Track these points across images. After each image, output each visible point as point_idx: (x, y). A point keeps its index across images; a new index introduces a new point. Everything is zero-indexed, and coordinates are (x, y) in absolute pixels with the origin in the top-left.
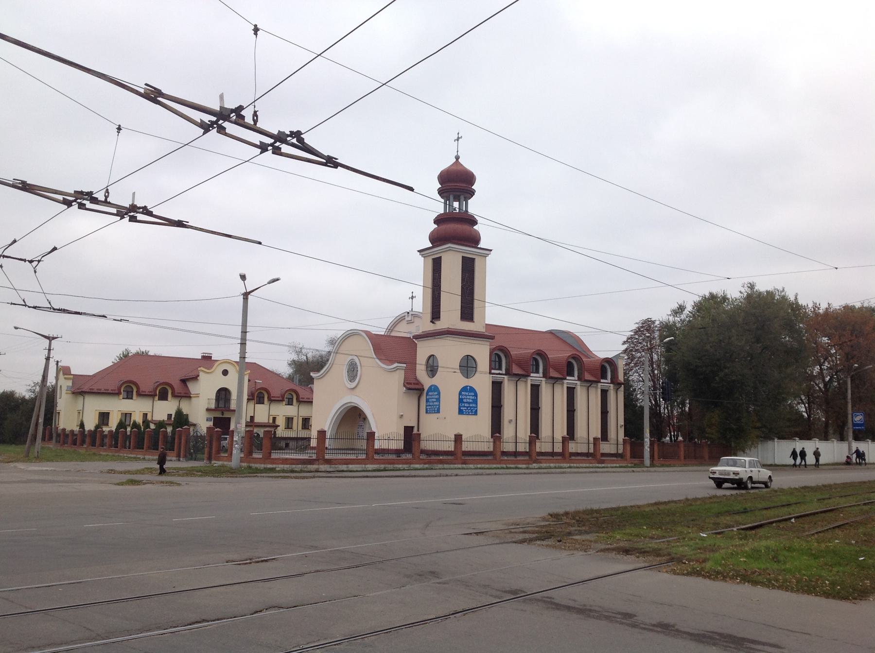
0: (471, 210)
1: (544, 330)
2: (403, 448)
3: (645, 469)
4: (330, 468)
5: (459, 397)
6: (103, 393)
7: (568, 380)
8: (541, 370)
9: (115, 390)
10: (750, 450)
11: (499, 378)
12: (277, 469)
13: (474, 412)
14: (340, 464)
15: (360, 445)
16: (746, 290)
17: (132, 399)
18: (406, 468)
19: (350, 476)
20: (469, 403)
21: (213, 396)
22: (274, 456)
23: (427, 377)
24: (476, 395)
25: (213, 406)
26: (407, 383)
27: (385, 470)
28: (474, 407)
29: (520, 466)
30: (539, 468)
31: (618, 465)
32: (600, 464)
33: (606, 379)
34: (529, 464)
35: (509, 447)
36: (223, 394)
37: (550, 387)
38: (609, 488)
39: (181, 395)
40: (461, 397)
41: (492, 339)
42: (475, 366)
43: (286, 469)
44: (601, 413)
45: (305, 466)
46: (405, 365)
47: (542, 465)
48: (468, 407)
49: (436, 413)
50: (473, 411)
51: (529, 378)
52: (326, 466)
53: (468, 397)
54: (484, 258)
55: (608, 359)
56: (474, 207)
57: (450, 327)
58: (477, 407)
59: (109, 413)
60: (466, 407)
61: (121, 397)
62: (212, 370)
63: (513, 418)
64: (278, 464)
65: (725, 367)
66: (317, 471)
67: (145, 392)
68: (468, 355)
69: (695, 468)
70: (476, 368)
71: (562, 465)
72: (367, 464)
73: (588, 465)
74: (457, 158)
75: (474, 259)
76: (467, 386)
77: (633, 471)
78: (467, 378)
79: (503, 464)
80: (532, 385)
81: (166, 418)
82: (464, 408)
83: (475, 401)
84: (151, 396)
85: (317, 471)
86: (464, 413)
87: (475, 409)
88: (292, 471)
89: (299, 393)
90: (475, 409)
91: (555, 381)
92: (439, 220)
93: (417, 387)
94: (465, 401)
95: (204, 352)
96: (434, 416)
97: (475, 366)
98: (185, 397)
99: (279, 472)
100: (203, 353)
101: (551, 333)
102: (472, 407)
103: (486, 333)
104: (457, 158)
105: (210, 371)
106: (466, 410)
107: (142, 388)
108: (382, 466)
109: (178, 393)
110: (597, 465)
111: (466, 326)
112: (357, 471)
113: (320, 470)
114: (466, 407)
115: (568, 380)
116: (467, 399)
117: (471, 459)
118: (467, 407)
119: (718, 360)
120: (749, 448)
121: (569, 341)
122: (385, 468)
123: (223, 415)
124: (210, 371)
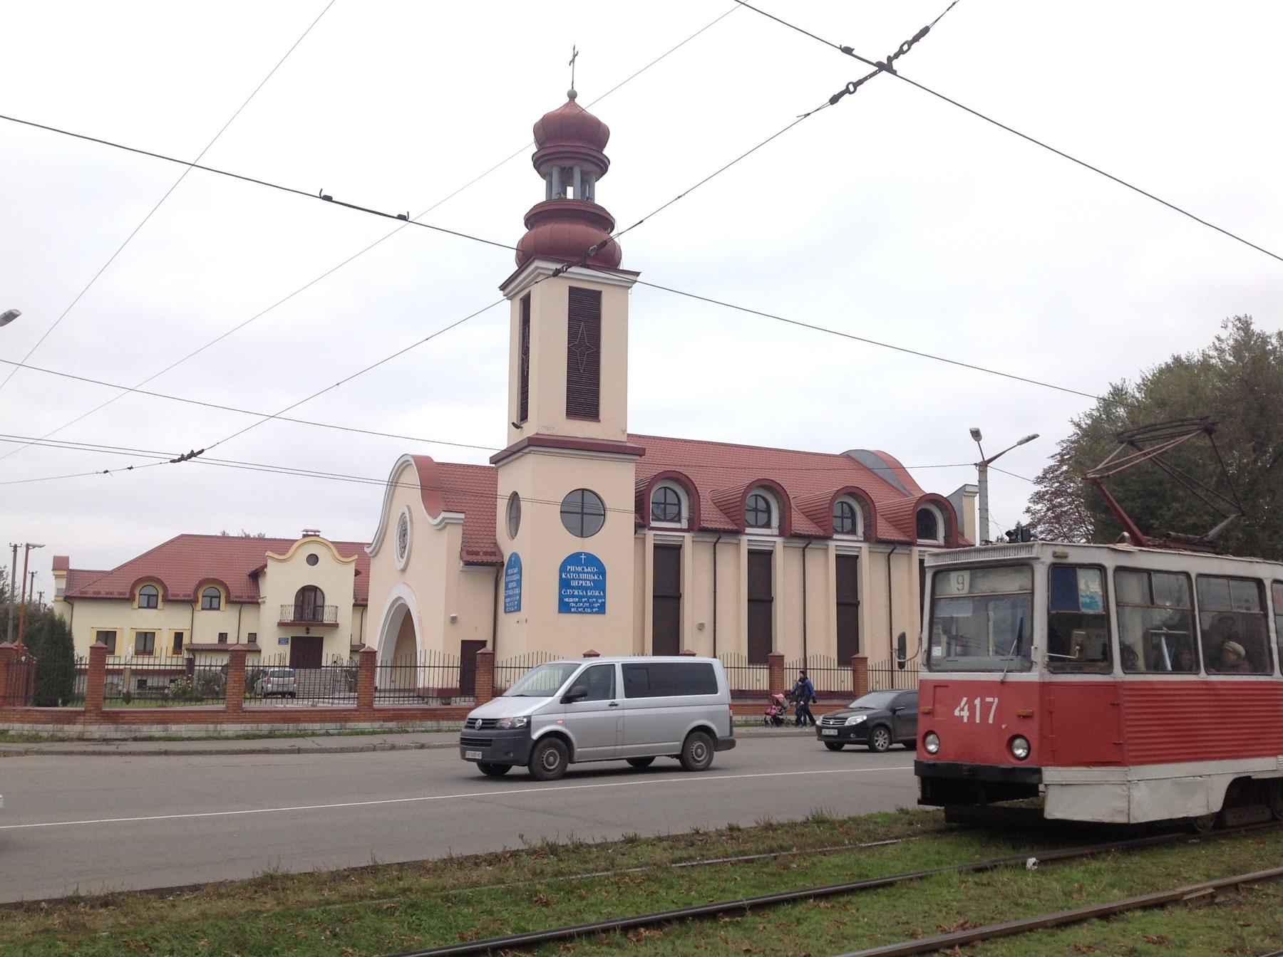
1: (838, 453)
2: (458, 686)
4: (116, 731)
5: (561, 576)
6: (115, 599)
7: (836, 540)
8: (775, 521)
11: (671, 538)
12: (11, 733)
13: (598, 607)
14: (146, 723)
15: (504, 680)
16: (1230, 336)
18: (331, 732)
20: (586, 589)
21: (291, 601)
22: (248, 705)
24: (602, 571)
25: (290, 617)
26: (469, 553)
27: (271, 735)
28: (597, 597)
33: (935, 538)
36: (309, 599)
38: (808, 772)
39: (241, 600)
40: (564, 576)
41: (641, 456)
42: (603, 513)
43: (25, 733)
45: (60, 726)
46: (462, 516)
50: (596, 605)
54: (623, 290)
55: (936, 498)
58: (604, 597)
60: (576, 596)
61: (136, 605)
62: (287, 556)
63: (707, 620)
64: (12, 721)
65: (1175, 499)
67: (177, 595)
68: (583, 490)
70: (604, 515)
72: (221, 723)
74: (572, 95)
75: (600, 293)
76: (580, 554)
78: (582, 536)
80: (750, 552)
81: (216, 641)
82: (571, 600)
83: (601, 585)
84: (190, 602)
86: (573, 610)
87: (600, 601)
88: (36, 739)
89: (149, 575)
90: (600, 601)
91: (805, 541)
92: (534, 218)
93: (493, 559)
94: (574, 583)
96: (514, 617)
97: (603, 513)
98: (249, 603)
99: (13, 740)
101: (847, 456)
102: (592, 597)
103: (628, 444)
104: (572, 95)
105: (282, 557)
106: (576, 603)
107: (234, 593)
108: (265, 727)
109: (236, 597)
112: (189, 739)
113: (87, 735)
114: (576, 596)
115: (836, 540)
118: (581, 597)
119: (1160, 483)
121: (886, 475)
122: (270, 732)
123: (308, 633)
124: (282, 557)
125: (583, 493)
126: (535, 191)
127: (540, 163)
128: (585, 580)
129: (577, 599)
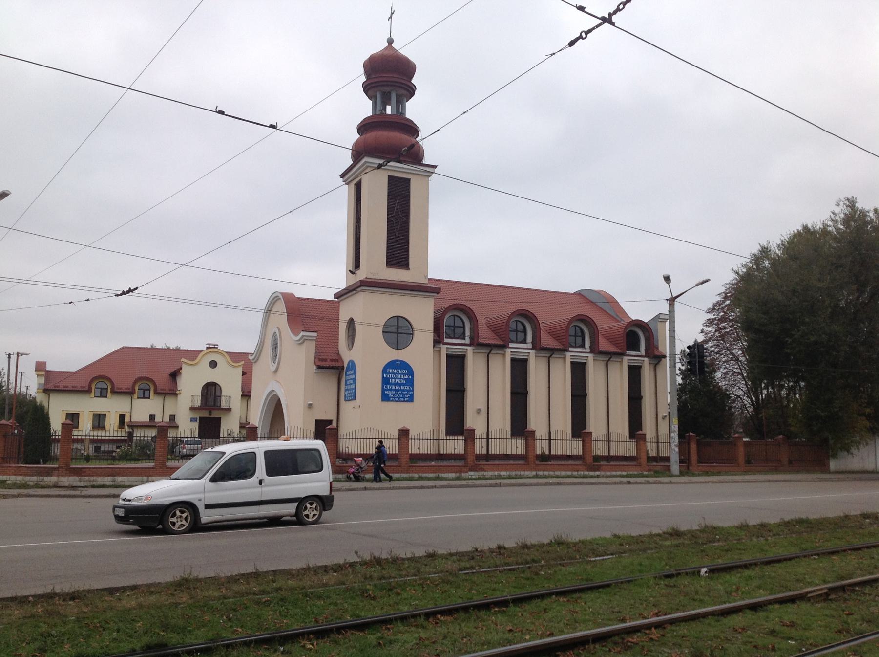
0: (409, 114)
3: (674, 479)
4: (80, 481)
6: (78, 391)
8: (529, 338)
9: (84, 387)
10: (858, 449)
11: (458, 350)
12: (9, 482)
14: (100, 476)
16: (841, 211)
17: (106, 397)
19: (96, 494)
20: (400, 385)
23: (346, 350)
24: (411, 373)
25: (198, 404)
28: (408, 391)
29: (445, 475)
30: (479, 478)
31: (624, 473)
32: (592, 471)
33: (639, 351)
34: (461, 472)
35: (599, 449)
36: (211, 391)
37: (543, 364)
41: (438, 293)
43: (18, 482)
44: (572, 396)
46: (315, 334)
47: (485, 473)
48: (399, 390)
49: (407, 401)
50: (407, 396)
51: (508, 350)
52: (71, 478)
53: (399, 376)
55: (639, 322)
56: (413, 110)
57: (370, 276)
58: (413, 390)
59: (79, 413)
60: (393, 390)
61: (92, 395)
64: (9, 475)
66: (56, 486)
67: (121, 388)
68: (398, 317)
69: (770, 477)
70: (412, 334)
71: (522, 473)
73: (569, 473)
74: (390, 41)
76: (396, 361)
77: (629, 483)
78: (397, 349)
79: (412, 472)
80: (513, 360)
82: (390, 392)
83: (410, 382)
84: (130, 393)
85: (56, 486)
86: (391, 399)
87: (410, 393)
88: (25, 486)
90: (410, 393)
91: (550, 352)
92: (364, 127)
94: (392, 381)
95: (209, 343)
99: (10, 487)
100: (208, 344)
101: (579, 294)
102: (404, 390)
103: (429, 285)
104: (390, 41)
106: (394, 395)
109: (162, 390)
110: (586, 473)
111: (397, 275)
113: (60, 484)
116: (396, 378)
117: (442, 464)
118: (396, 391)
120: (857, 446)
123: (210, 415)
125: (398, 319)
126: (365, 108)
127: (368, 88)
128: (399, 379)
129: (394, 392)
